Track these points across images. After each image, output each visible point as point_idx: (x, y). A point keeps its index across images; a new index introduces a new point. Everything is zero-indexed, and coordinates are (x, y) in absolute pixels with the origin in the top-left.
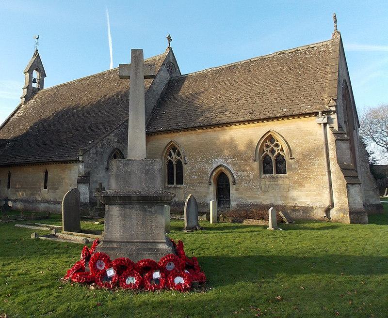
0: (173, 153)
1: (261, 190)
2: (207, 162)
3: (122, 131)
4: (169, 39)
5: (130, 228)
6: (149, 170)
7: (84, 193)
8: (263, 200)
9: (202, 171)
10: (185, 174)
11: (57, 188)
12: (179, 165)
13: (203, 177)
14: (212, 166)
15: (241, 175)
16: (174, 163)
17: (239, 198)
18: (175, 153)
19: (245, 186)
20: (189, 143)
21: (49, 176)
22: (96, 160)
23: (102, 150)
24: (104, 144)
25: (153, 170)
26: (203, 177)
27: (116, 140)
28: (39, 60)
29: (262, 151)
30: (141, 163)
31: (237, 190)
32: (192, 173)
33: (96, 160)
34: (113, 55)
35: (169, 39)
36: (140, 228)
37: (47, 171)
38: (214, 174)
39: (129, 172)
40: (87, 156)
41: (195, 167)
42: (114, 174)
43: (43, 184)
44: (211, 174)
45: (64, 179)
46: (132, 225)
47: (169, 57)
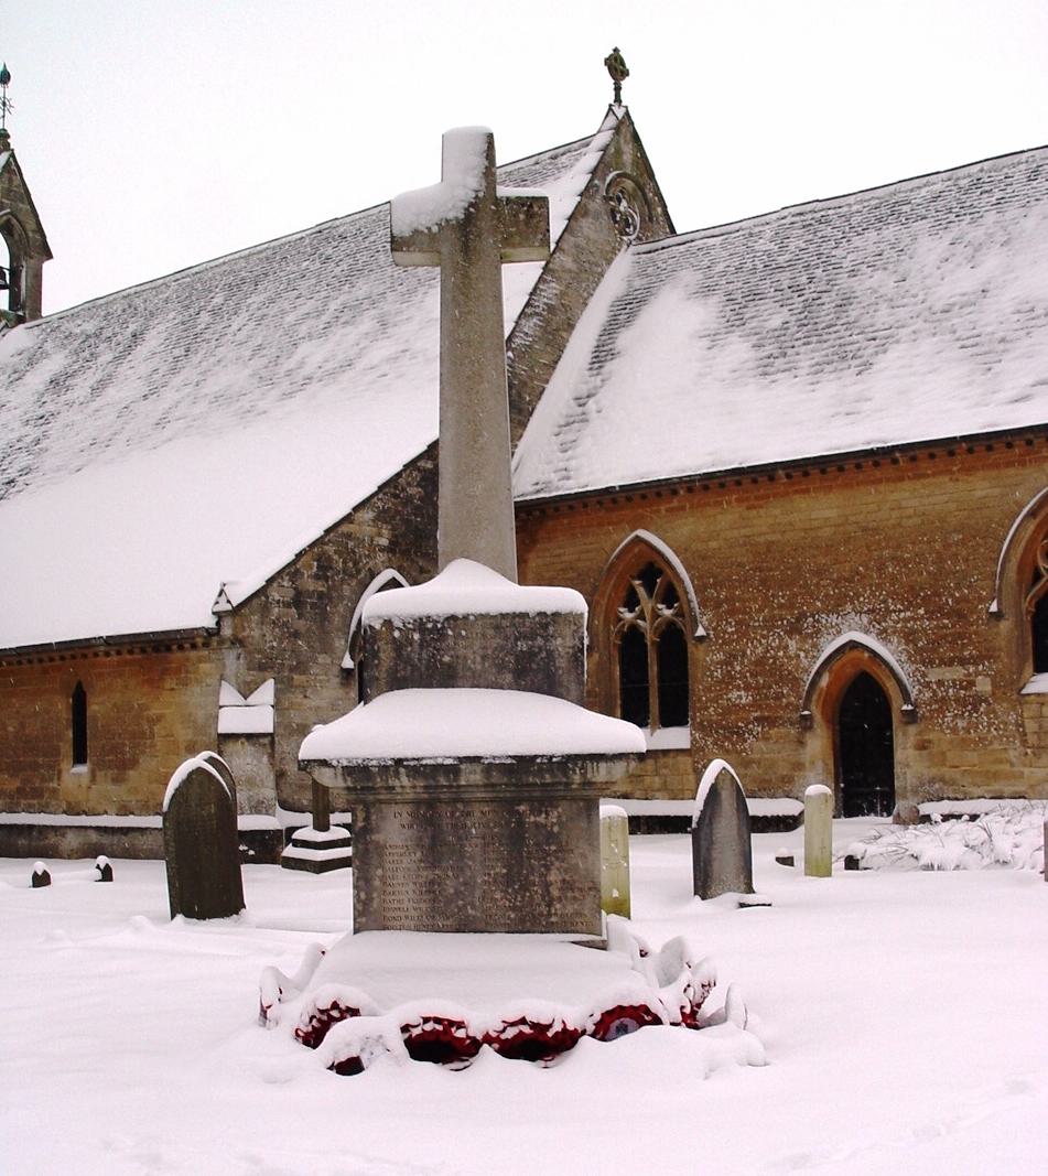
0: (641, 592)
1: (1024, 742)
2: (794, 630)
3: (409, 499)
4: (616, 67)
5: (457, 892)
6: (531, 655)
7: (251, 782)
8: (1032, 786)
9: (771, 672)
10: (699, 687)
11: (134, 763)
12: (674, 641)
13: (779, 696)
14: (815, 646)
15: (940, 683)
16: (650, 638)
17: (932, 781)
18: (650, 592)
19: (954, 730)
20: (713, 544)
21: (95, 708)
22: (296, 635)
23: (321, 587)
24: (330, 559)
25: (550, 654)
26: (779, 696)
27: (384, 542)
28: (17, 181)
29: (1029, 575)
30: (497, 628)
31: (922, 746)
32: (728, 681)
33: (296, 635)
34: (626, 545)
35: (616, 67)
36: (498, 896)
37: (79, 685)
38: (825, 681)
39: (449, 666)
40: (255, 618)
41: (744, 654)
42: (383, 675)
43: (67, 748)
44: (814, 683)
45: (159, 718)
46: (465, 884)
47: (619, 152)
